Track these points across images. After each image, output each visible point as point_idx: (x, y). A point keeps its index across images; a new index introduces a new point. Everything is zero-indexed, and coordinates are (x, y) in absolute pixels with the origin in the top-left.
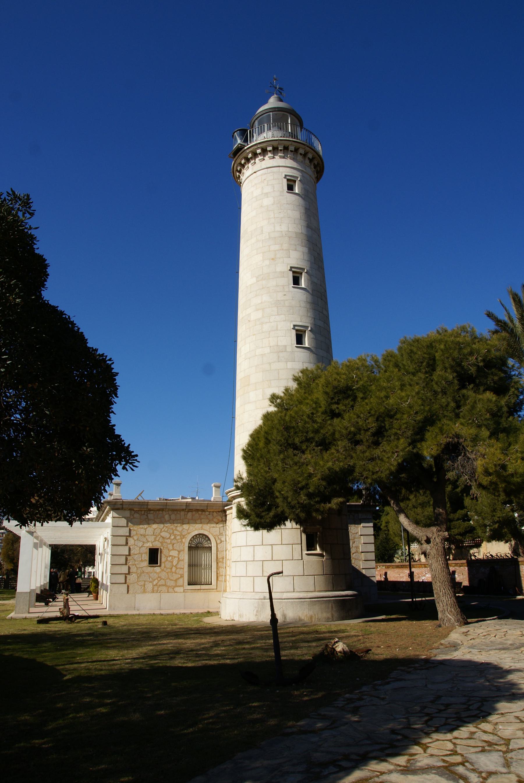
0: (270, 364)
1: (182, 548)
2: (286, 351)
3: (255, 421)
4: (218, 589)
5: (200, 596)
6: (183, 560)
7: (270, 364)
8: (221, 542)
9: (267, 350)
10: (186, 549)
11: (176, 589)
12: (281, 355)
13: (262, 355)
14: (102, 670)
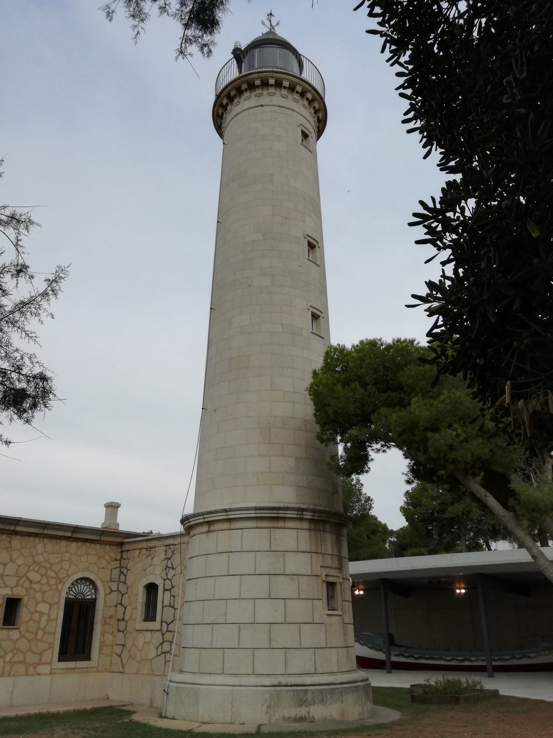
11: (40, 669)
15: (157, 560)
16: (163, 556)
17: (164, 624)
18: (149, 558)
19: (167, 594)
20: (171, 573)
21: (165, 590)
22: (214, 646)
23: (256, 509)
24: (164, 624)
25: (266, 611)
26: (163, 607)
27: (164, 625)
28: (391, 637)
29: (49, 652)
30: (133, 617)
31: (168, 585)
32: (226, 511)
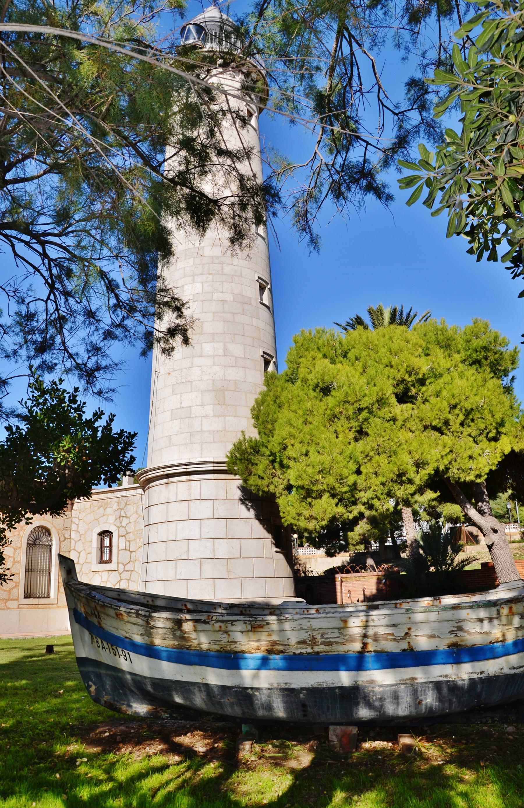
0: (233, 314)
1: (19, 545)
2: (251, 304)
3: (213, 381)
4: (59, 605)
5: (37, 614)
6: (19, 562)
7: (233, 314)
8: (65, 539)
9: (229, 297)
10: (24, 546)
11: (10, 604)
12: (246, 307)
13: (224, 302)
14: (167, 783)
15: (109, 510)
16: (115, 507)
17: (120, 565)
18: (102, 509)
19: (122, 540)
20: (125, 522)
21: (119, 536)
22: (178, 578)
23: (214, 463)
24: (120, 565)
25: (223, 549)
26: (118, 551)
27: (121, 566)
28: (391, 367)
29: (16, 590)
30: (88, 561)
31: (122, 532)
32: (185, 464)
